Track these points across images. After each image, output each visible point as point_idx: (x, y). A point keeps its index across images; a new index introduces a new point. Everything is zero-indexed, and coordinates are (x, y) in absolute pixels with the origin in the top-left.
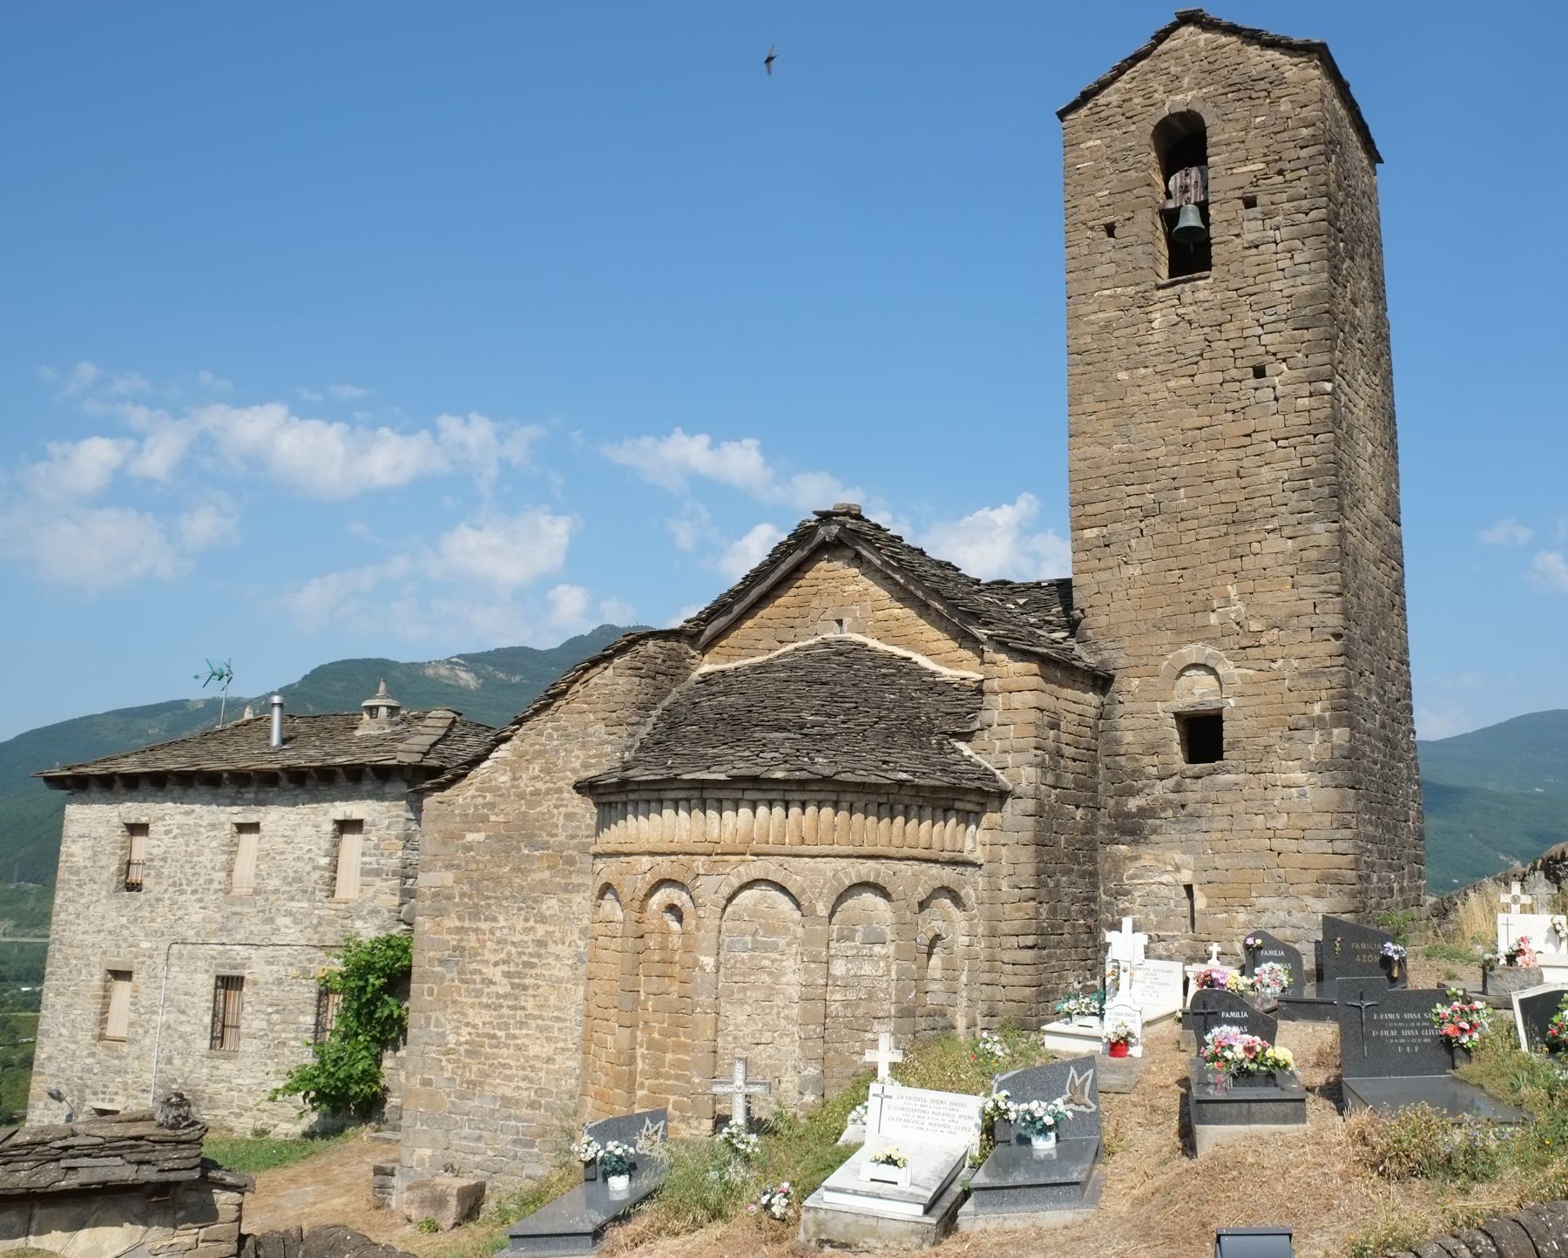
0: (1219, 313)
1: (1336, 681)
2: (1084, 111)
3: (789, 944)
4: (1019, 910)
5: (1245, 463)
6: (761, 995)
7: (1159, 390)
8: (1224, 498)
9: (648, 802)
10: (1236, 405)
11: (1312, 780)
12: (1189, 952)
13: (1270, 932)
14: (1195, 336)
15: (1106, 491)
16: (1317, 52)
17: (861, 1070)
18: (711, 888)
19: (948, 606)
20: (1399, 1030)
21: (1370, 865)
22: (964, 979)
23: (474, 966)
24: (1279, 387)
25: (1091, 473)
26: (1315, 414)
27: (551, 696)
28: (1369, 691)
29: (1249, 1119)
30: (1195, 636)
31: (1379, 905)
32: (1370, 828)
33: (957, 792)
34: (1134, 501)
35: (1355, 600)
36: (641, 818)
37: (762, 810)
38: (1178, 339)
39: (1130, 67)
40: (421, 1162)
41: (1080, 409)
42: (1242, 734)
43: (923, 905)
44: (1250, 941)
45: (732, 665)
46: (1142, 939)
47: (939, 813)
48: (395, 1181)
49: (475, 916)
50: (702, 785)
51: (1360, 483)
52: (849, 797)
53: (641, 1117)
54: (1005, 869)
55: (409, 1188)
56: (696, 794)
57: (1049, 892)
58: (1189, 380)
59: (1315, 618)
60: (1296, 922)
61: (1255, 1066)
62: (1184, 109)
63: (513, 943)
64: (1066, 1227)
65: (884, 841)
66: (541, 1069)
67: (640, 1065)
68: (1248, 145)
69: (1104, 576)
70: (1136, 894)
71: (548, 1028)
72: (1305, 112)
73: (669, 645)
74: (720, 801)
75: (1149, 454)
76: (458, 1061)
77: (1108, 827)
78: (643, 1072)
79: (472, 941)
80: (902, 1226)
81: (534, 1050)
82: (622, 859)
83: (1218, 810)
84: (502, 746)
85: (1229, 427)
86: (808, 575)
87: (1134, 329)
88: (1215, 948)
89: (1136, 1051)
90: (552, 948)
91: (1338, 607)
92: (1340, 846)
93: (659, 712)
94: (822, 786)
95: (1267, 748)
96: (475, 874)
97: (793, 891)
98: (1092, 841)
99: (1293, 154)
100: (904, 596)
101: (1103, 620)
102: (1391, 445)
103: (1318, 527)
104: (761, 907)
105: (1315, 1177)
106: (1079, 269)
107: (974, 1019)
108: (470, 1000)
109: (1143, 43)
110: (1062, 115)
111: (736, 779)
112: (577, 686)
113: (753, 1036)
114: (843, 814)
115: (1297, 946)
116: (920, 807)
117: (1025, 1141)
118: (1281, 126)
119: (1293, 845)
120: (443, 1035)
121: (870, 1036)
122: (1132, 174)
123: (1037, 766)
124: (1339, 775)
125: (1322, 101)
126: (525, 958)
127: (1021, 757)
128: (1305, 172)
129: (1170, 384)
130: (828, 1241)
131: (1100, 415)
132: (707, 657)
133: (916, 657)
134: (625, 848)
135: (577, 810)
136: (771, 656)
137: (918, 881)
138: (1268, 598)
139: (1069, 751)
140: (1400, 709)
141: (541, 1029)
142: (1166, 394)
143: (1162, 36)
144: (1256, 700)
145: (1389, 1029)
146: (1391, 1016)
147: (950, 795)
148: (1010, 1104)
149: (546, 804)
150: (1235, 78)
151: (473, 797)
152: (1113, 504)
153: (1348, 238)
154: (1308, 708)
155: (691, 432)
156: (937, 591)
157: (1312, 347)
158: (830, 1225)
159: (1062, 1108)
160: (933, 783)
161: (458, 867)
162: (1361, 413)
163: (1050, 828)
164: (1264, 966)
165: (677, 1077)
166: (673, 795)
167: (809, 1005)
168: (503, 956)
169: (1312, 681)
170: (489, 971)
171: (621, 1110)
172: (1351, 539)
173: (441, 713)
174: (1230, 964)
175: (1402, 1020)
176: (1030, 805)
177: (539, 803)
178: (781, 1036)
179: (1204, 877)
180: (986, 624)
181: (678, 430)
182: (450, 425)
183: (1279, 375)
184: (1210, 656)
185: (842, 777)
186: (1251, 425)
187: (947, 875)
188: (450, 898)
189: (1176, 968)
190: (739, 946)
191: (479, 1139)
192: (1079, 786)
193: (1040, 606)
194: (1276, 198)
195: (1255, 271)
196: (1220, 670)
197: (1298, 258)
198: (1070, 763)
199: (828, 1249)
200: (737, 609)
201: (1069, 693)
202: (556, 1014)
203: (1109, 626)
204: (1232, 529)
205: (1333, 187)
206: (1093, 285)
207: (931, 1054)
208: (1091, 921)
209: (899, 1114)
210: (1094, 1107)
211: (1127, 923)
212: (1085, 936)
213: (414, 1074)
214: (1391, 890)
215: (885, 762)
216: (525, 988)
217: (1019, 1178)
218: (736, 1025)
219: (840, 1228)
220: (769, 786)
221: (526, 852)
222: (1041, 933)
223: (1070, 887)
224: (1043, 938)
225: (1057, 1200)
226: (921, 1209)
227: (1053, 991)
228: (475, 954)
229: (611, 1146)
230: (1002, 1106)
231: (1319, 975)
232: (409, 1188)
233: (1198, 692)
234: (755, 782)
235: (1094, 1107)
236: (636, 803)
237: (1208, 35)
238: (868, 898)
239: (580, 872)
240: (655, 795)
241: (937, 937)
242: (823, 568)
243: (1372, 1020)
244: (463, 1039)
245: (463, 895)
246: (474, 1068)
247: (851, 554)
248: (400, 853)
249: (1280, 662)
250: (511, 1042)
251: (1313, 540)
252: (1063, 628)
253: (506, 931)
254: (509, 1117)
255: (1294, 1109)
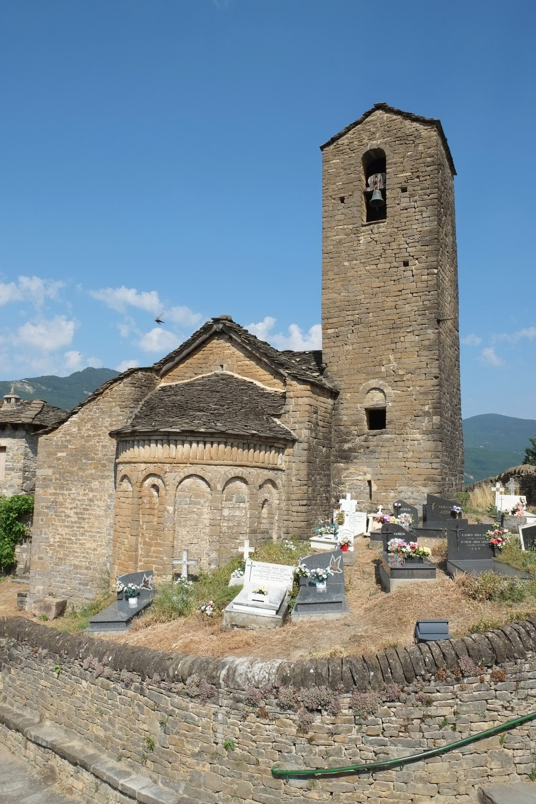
0: (389, 238)
1: (435, 396)
2: (332, 147)
3: (205, 502)
4: (300, 489)
5: (399, 303)
6: (193, 523)
7: (362, 270)
8: (389, 318)
9: (144, 440)
10: (395, 278)
11: (424, 438)
12: (369, 509)
13: (404, 500)
14: (379, 247)
15: (338, 313)
16: (436, 124)
17: (235, 555)
18: (172, 478)
19: (270, 360)
20: (472, 541)
21: (446, 474)
22: (276, 518)
23: (61, 509)
24: (414, 270)
25: (331, 305)
26: (429, 283)
27: (96, 395)
28: (447, 401)
29: (412, 576)
30: (375, 376)
31: (448, 490)
32: (446, 459)
33: (276, 439)
34: (350, 318)
35: (443, 362)
36: (141, 447)
37: (194, 445)
38: (371, 248)
39: (353, 128)
40: (38, 592)
41: (327, 277)
42: (394, 418)
43: (261, 487)
44: (396, 504)
45: (174, 384)
46: (355, 502)
47: (268, 448)
48: (27, 599)
49: (62, 488)
50: (169, 434)
51: (446, 312)
52: (231, 440)
53: (142, 574)
54: (294, 472)
55: (35, 602)
56: (166, 437)
57: (312, 482)
58: (375, 267)
59: (427, 370)
60: (415, 497)
61: (415, 555)
62: (376, 147)
63: (79, 500)
64: (337, 620)
65: (245, 459)
66: (91, 553)
67: (140, 552)
68: (404, 164)
69: (336, 349)
70: (347, 484)
71: (94, 536)
72: (429, 151)
73: (147, 374)
74: (176, 441)
75: (357, 298)
76: (54, 549)
77: (335, 456)
78: (141, 555)
79: (60, 499)
80: (267, 619)
81: (88, 545)
82: (132, 465)
83: (383, 449)
84: (74, 416)
85: (393, 288)
86: (208, 346)
87: (352, 244)
88: (380, 507)
89: (351, 549)
90: (96, 502)
91: (437, 365)
92: (435, 466)
93: (143, 402)
94: (220, 435)
95: (405, 424)
96: (62, 471)
97: (207, 479)
98: (329, 461)
99: (424, 169)
100: (250, 356)
101: (335, 368)
102: (456, 297)
103: (429, 331)
104: (193, 486)
105: (445, 600)
106: (328, 217)
107: (280, 535)
108: (59, 524)
109: (359, 117)
110: (322, 148)
111: (184, 431)
112: (107, 391)
113: (190, 540)
114: (229, 447)
115: (415, 506)
116: (260, 445)
117: (313, 585)
118: (419, 157)
119: (415, 465)
120: (48, 538)
121: (238, 541)
122: (353, 175)
123: (309, 429)
124: (436, 436)
125: (437, 146)
126: (84, 506)
127: (302, 425)
128: (428, 177)
129: (367, 268)
130: (235, 625)
131: (336, 280)
132: (163, 380)
133: (255, 382)
134: (134, 460)
135: (107, 444)
136: (192, 380)
137: (259, 477)
138: (407, 361)
139: (321, 423)
140: (457, 410)
141: (91, 536)
142: (365, 272)
143: (368, 114)
144: (400, 404)
145: (468, 540)
146: (469, 535)
147: (273, 441)
148: (306, 570)
149: (93, 441)
150: (399, 134)
151: (61, 437)
152: (341, 319)
153: (444, 207)
154: (423, 408)
155: (129, 287)
156: (265, 354)
157: (429, 254)
158: (237, 618)
159: (329, 571)
160: (266, 435)
161: (54, 467)
162: (447, 284)
163: (313, 456)
164: (402, 514)
165: (156, 557)
166: (155, 438)
167: (213, 528)
168: (74, 505)
169: (425, 396)
170: (68, 512)
171: (131, 571)
172: (442, 337)
173: (38, 402)
174: (386, 514)
175: (474, 537)
176: (306, 446)
177: (90, 441)
178: (201, 541)
179: (376, 477)
180: (287, 368)
181: (123, 286)
182: (24, 280)
183: (415, 265)
184: (381, 385)
185: (229, 432)
186: (401, 287)
187: (270, 474)
188: (51, 480)
189: (364, 515)
190: (184, 503)
191: (64, 582)
192: (325, 438)
193: (306, 362)
194: (415, 188)
195: (405, 220)
196: (385, 391)
197: (424, 215)
198: (321, 428)
199: (235, 628)
200: (177, 359)
201: (322, 399)
202: (98, 530)
203: (338, 371)
204: (392, 331)
205: (440, 184)
206: (334, 224)
207: (267, 549)
208: (327, 495)
209: (259, 573)
210: (341, 571)
211: (349, 496)
212: (325, 501)
213: (35, 555)
214: (453, 484)
215: (246, 426)
216: (84, 519)
217: (310, 600)
218: (182, 536)
219: (241, 620)
220: (198, 435)
221: (84, 461)
222: (309, 499)
223: (320, 480)
224: (310, 502)
225: (332, 609)
226: (275, 612)
227: (313, 524)
228: (62, 504)
229: (130, 585)
230: (303, 570)
231: (425, 519)
232: (35, 602)
233: (375, 400)
234: (192, 433)
235: (341, 571)
236: (138, 441)
237: (388, 115)
238: (238, 483)
239: (108, 470)
240: (147, 438)
241: (266, 500)
242: (216, 343)
243: (461, 536)
244: (56, 540)
245: (56, 479)
246: (62, 553)
247: (227, 337)
248: (22, 461)
249: (412, 388)
250: (78, 542)
251: (427, 336)
252: (317, 371)
253: (75, 495)
254: (77, 573)
255: (430, 572)
